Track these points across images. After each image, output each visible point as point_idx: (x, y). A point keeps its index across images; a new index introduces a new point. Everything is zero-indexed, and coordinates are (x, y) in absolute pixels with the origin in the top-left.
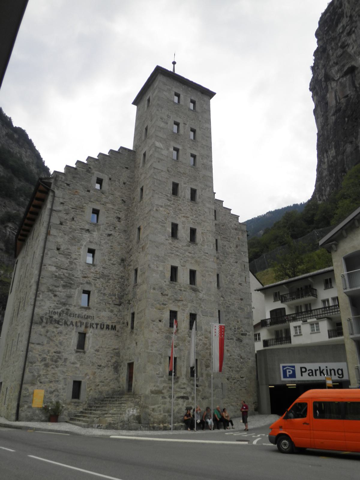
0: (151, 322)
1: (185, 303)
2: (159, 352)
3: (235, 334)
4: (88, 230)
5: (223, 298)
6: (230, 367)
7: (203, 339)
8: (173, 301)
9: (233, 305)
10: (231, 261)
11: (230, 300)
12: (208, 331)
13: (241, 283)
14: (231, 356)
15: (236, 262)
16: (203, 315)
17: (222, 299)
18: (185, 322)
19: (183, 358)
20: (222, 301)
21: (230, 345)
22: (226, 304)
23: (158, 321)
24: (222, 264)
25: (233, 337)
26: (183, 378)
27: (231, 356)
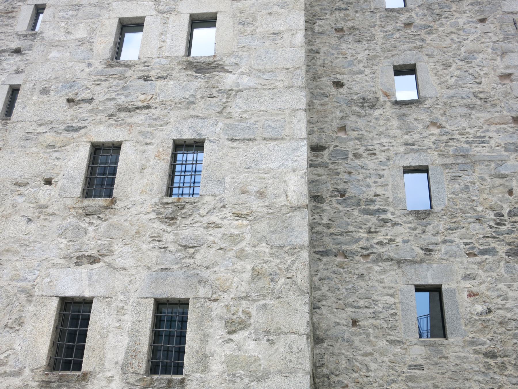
0: (13, 187)
1: (156, 113)
2: (22, 284)
3: (501, 234)
4: (18, 51)
5: (440, 127)
6: (493, 355)
7: (226, 222)
8: (111, 116)
9: (483, 142)
10: (461, 22)
11: (468, 130)
12: (253, 188)
13: (508, 71)
14: (489, 311)
15: (482, 21)
16: (233, 140)
17: (435, 131)
18: (148, 171)
19: (121, 297)
20: (433, 138)
21: (480, 272)
22: (452, 143)
23: (39, 182)
24: (423, 36)
25: (493, 244)
26: (110, 379)
27: (489, 311)
